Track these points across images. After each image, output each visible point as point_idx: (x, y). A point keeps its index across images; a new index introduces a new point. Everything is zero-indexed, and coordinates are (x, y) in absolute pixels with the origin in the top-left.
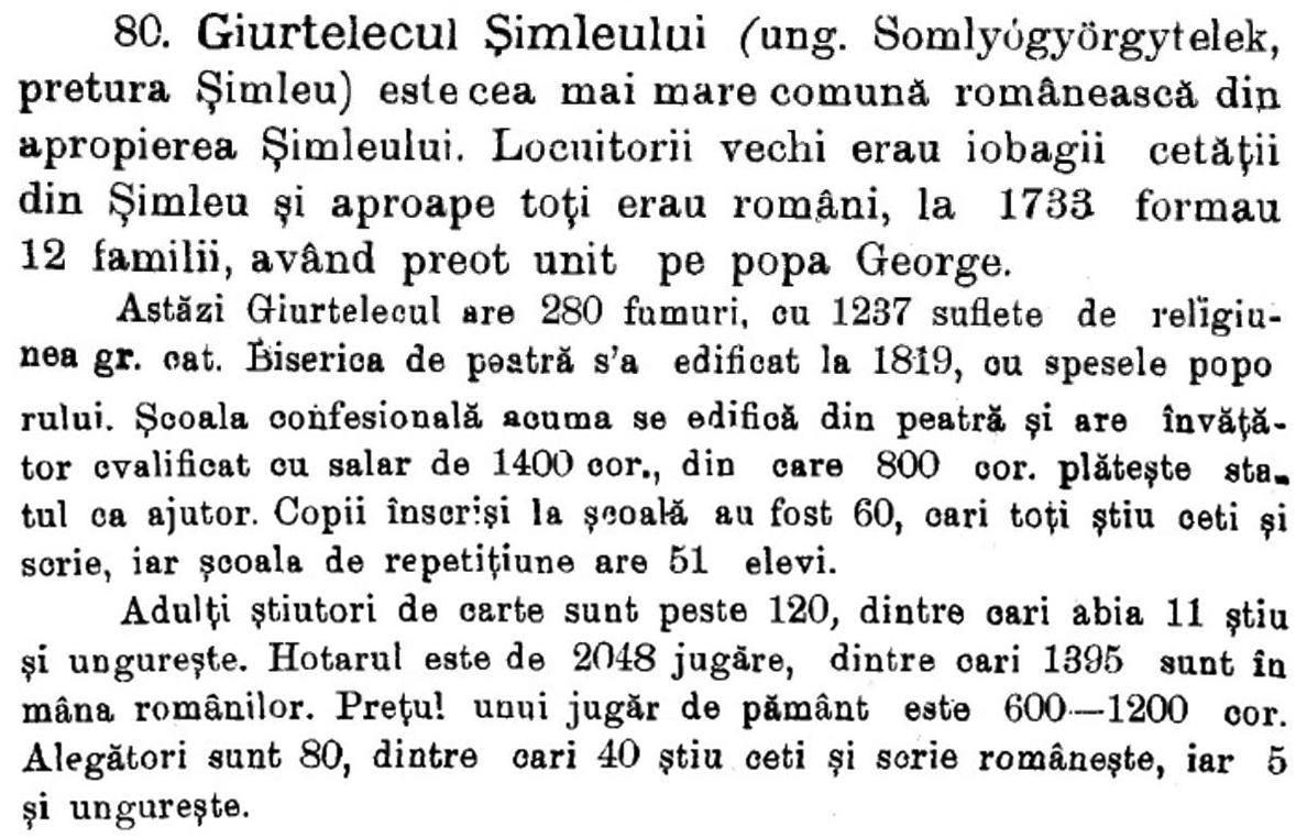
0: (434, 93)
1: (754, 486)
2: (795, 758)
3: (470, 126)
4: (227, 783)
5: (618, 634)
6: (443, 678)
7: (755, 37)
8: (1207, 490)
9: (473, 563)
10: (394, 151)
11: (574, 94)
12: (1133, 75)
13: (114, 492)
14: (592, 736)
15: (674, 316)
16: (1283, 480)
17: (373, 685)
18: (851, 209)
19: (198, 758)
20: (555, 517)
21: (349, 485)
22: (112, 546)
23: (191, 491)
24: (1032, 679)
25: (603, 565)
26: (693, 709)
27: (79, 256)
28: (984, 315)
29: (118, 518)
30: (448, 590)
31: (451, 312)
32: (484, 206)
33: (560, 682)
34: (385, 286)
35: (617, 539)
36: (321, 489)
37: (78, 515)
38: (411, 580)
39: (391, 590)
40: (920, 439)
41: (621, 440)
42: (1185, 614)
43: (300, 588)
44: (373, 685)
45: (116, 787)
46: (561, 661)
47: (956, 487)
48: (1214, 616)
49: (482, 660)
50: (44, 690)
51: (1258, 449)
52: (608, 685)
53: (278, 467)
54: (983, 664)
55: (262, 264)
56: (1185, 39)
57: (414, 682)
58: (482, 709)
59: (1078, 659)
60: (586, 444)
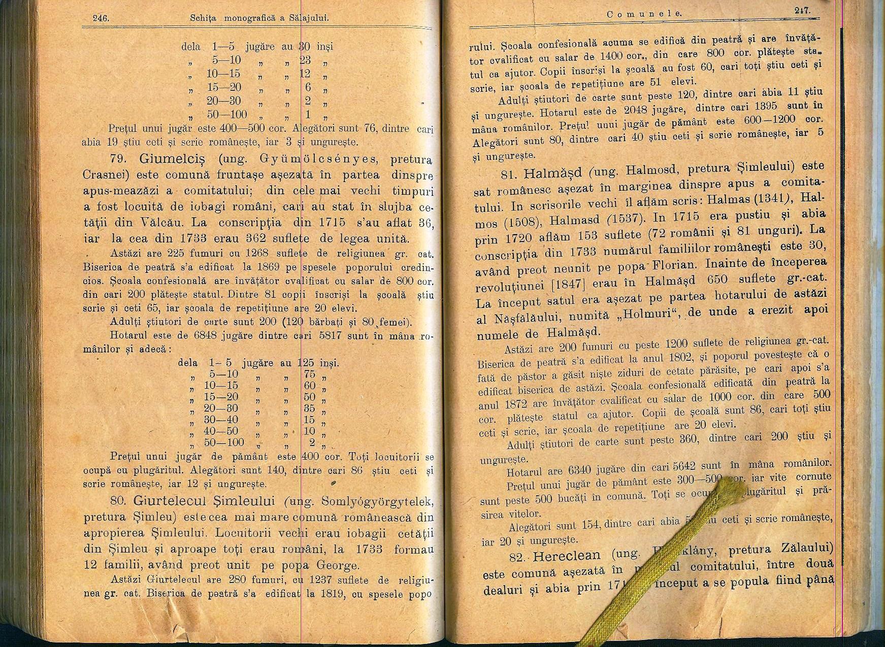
0: (199, 518)
1: (673, 60)
2: (685, 136)
3: (209, 527)
4: (530, 149)
5: (636, 104)
6: (588, 117)
7: (288, 501)
8: (799, 56)
9: (596, 85)
10: (187, 534)
11: (237, 518)
12: (394, 513)
13: (494, 68)
14: (631, 131)
15: (266, 581)
16: (820, 53)
17: (568, 119)
18: (315, 550)
19: (521, 142)
20: (618, 71)
21: (561, 63)
22: (496, 83)
23: (518, 67)
24: (752, 112)
25: (632, 84)
26: (658, 123)
27: (101, 564)
28: (353, 581)
29: (497, 75)
30: (589, 92)
31: (204, 580)
32: (213, 550)
33: (621, 117)
34: (186, 572)
35: (636, 77)
36: (553, 65)
37: (486, 75)
38: (578, 90)
39: (573, 93)
40: (719, 46)
41: (635, 49)
42: (794, 91)
43: (548, 93)
44: (568, 119)
45: (498, 151)
46: (621, 111)
47: (728, 59)
48: (801, 92)
49: (599, 112)
50: (478, 125)
51: (813, 45)
52: (636, 118)
53: (541, 59)
54: (738, 108)
55: (151, 566)
56: (408, 503)
57: (580, 119)
58: (600, 126)
59: (764, 106)
60: (627, 50)
